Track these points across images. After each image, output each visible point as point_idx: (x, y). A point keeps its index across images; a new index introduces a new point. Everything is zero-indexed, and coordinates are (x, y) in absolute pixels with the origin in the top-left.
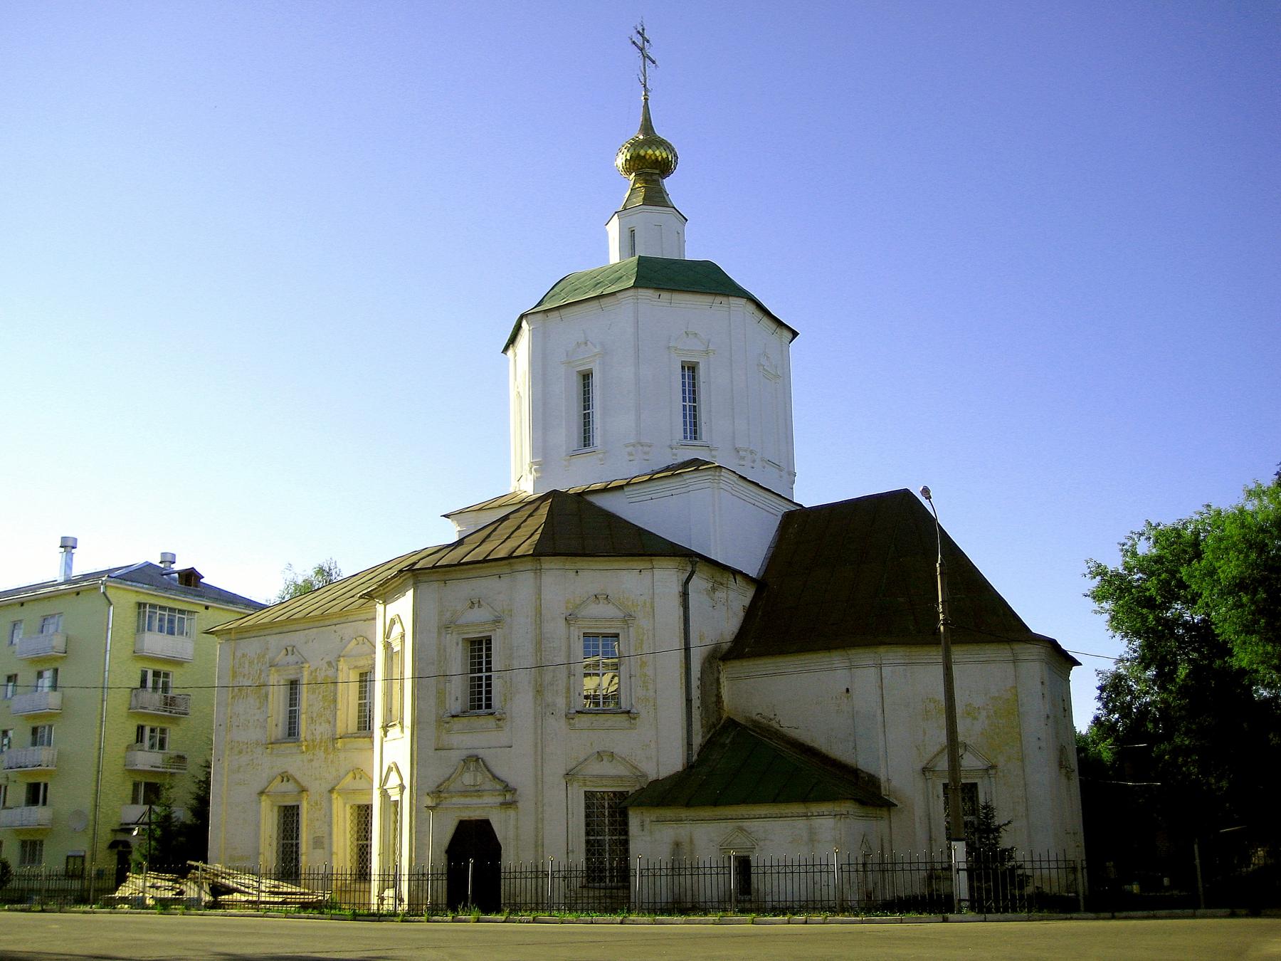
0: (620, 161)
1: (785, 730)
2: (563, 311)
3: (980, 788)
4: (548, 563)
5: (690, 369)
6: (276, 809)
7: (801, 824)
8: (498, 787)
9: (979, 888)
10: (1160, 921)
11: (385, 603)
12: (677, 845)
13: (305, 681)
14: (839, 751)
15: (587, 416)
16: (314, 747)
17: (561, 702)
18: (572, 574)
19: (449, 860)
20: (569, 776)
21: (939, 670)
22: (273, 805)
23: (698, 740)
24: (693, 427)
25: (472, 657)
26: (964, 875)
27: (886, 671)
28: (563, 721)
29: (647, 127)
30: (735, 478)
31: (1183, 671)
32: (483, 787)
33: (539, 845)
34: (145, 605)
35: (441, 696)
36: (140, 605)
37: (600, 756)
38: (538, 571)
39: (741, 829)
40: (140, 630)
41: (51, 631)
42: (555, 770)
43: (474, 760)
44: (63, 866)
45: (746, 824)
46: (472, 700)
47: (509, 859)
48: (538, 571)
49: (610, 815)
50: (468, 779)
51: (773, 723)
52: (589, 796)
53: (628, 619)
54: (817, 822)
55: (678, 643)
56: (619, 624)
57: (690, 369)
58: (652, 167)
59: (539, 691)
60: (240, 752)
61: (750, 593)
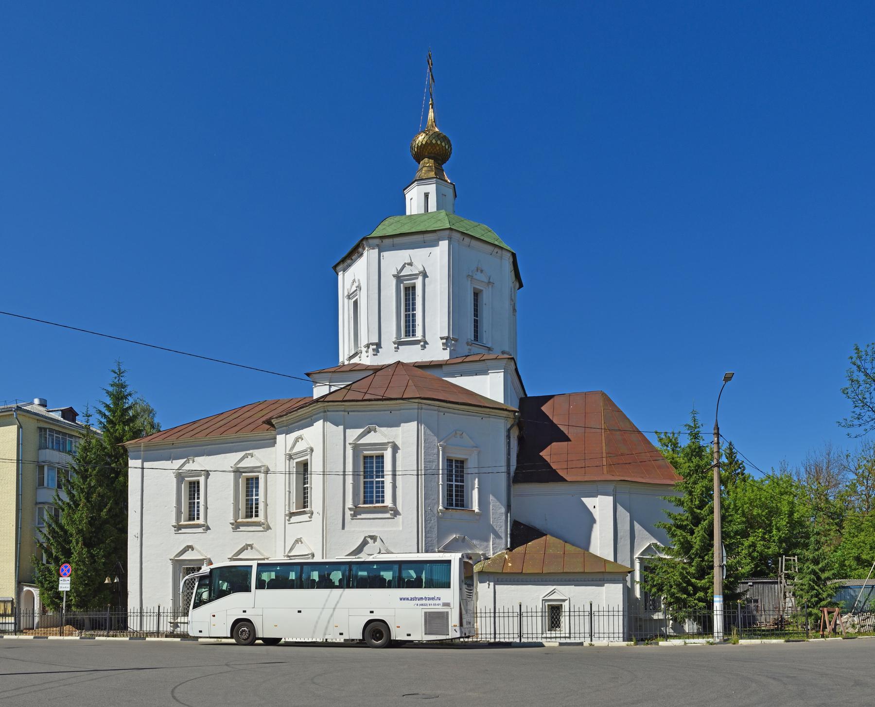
3: (484, 292)
5: (401, 599)
9: (729, 617)
10: (631, 419)
11: (344, 270)
13: (605, 467)
15: (476, 315)
17: (179, 620)
21: (144, 607)
23: (513, 468)
25: (462, 496)
26: (687, 641)
29: (119, 397)
30: (514, 368)
31: (65, 585)
34: (45, 429)
36: (40, 429)
40: (42, 447)
44: (260, 636)
46: (247, 512)
52: (426, 613)
55: (136, 672)
57: (401, 599)
61: (385, 254)
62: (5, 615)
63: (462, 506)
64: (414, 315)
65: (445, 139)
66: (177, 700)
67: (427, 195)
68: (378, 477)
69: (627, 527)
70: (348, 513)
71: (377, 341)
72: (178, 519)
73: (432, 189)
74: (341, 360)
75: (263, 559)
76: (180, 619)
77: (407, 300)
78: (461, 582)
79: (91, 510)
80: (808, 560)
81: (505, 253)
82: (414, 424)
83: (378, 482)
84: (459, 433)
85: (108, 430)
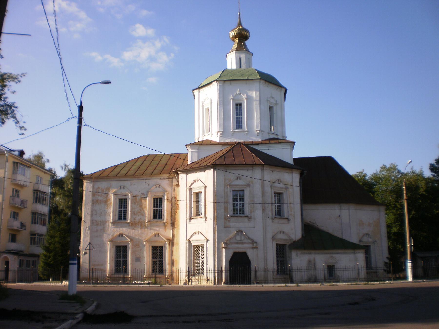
0: (232, 34)
1: (319, 227)
2: (232, 82)
4: (266, 168)
6: (114, 247)
7: (352, 256)
8: (250, 241)
12: (309, 261)
14: (337, 234)
16: (136, 224)
18: (271, 172)
19: (230, 265)
20: (273, 238)
22: (149, 246)
24: (239, 124)
27: (351, 211)
28: (271, 220)
32: (244, 241)
33: (265, 260)
35: (226, 209)
37: (280, 232)
38: (263, 170)
39: (332, 257)
41: (282, 186)
42: (269, 236)
43: (240, 232)
45: (334, 255)
47: (254, 265)
48: (263, 170)
49: (282, 250)
50: (238, 238)
51: (315, 225)
53: (286, 189)
54: (358, 255)
56: (284, 190)
58: (242, 37)
59: (264, 210)
60: (97, 225)
70: (188, 221)
74: (197, 136)
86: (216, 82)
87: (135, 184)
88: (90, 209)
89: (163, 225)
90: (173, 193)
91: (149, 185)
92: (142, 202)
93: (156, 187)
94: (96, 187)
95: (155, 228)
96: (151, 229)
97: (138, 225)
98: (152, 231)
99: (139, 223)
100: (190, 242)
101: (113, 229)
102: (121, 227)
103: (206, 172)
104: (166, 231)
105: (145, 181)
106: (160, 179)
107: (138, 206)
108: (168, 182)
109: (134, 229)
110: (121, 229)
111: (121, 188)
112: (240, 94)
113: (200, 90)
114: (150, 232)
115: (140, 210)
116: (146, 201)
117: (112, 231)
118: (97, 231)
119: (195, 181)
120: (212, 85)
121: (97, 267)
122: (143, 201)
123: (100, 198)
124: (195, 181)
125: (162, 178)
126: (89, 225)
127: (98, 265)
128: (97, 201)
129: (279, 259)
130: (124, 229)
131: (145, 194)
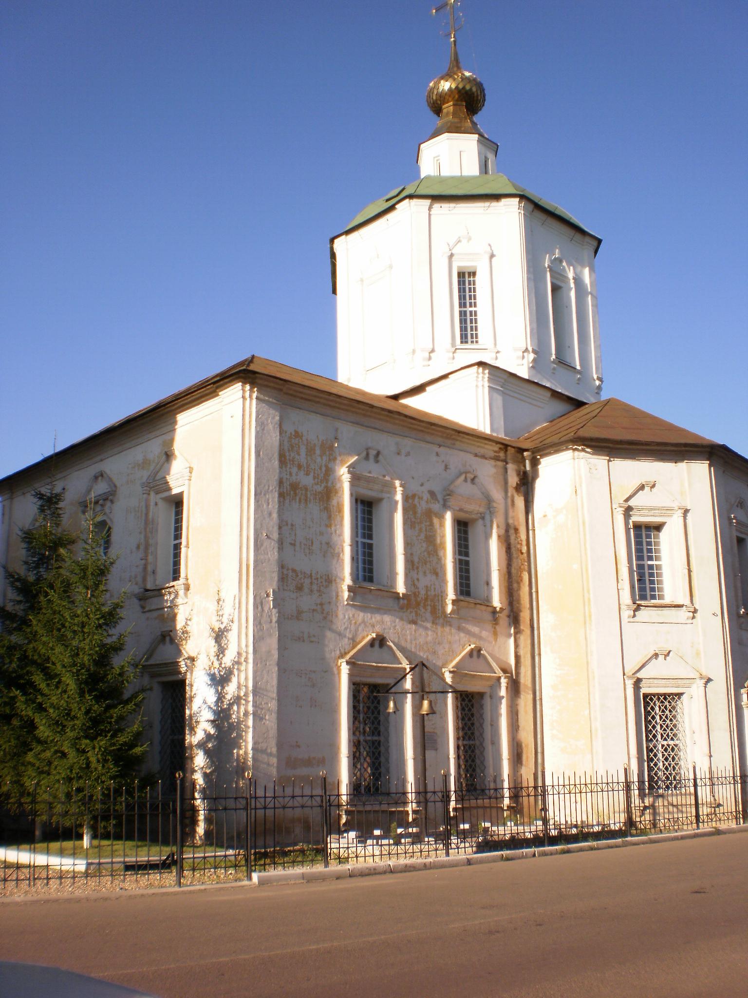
2: (551, 221)
24: (467, 330)
62: (562, 996)
63: (363, 502)
64: (461, 330)
65: (480, 85)
66: (491, 261)
67: (643, 535)
68: (471, 306)
69: (523, 670)
70: (627, 613)
71: (496, 448)
72: (453, 344)
73: (497, 233)
75: (494, 860)
76: (469, 309)
77: (463, 321)
78: (343, 505)
79: (108, 743)
80: (19, 775)
81: (587, 239)
82: (239, 385)
83: (471, 312)
84: (373, 453)
85: (462, 791)
86: (518, 199)
87: (408, 454)
88: (275, 515)
89: (489, 617)
90: (510, 511)
91: (446, 468)
92: (432, 524)
93: (466, 480)
94: (290, 429)
95: (475, 629)
96: (459, 629)
97: (425, 607)
98: (462, 635)
99: (426, 599)
100: (637, 683)
101: (351, 612)
102: (378, 610)
103: (683, 466)
104: (496, 640)
105: (436, 449)
106: (476, 455)
107: (422, 536)
108: (493, 471)
109: (414, 622)
110: (378, 617)
111: (367, 457)
112: (561, 261)
113: (437, 206)
114: (457, 638)
115: (429, 554)
116: (442, 525)
117: (354, 626)
118: (298, 615)
119: (642, 487)
120: (494, 204)
121: (303, 771)
122: (436, 521)
123: (307, 481)
124: (642, 487)
125: (481, 451)
126: (275, 585)
127: (309, 763)
128: (294, 487)
129: (362, 738)
130: (387, 618)
131: (440, 497)
